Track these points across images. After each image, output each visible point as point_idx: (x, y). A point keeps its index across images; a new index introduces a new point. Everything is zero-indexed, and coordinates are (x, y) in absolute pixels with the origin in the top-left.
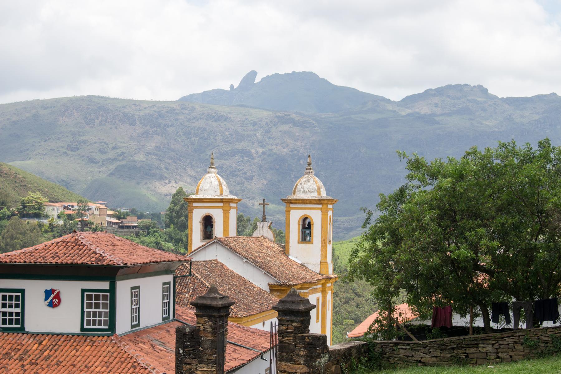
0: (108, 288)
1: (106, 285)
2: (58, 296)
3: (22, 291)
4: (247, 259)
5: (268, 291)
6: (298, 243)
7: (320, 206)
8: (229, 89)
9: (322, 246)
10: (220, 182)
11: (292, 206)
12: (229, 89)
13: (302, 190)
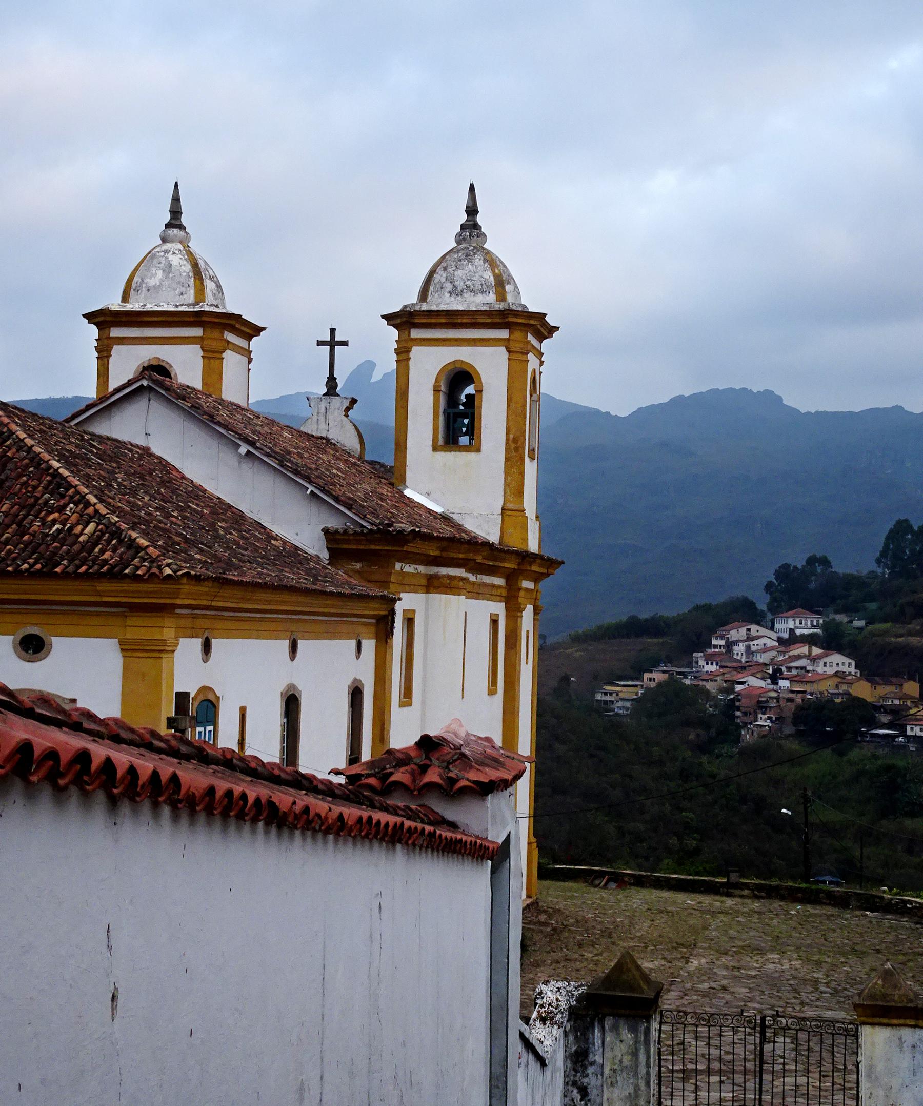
4: (252, 443)
5: (325, 555)
6: (435, 448)
7: (504, 334)
9: (507, 459)
13: (449, 287)
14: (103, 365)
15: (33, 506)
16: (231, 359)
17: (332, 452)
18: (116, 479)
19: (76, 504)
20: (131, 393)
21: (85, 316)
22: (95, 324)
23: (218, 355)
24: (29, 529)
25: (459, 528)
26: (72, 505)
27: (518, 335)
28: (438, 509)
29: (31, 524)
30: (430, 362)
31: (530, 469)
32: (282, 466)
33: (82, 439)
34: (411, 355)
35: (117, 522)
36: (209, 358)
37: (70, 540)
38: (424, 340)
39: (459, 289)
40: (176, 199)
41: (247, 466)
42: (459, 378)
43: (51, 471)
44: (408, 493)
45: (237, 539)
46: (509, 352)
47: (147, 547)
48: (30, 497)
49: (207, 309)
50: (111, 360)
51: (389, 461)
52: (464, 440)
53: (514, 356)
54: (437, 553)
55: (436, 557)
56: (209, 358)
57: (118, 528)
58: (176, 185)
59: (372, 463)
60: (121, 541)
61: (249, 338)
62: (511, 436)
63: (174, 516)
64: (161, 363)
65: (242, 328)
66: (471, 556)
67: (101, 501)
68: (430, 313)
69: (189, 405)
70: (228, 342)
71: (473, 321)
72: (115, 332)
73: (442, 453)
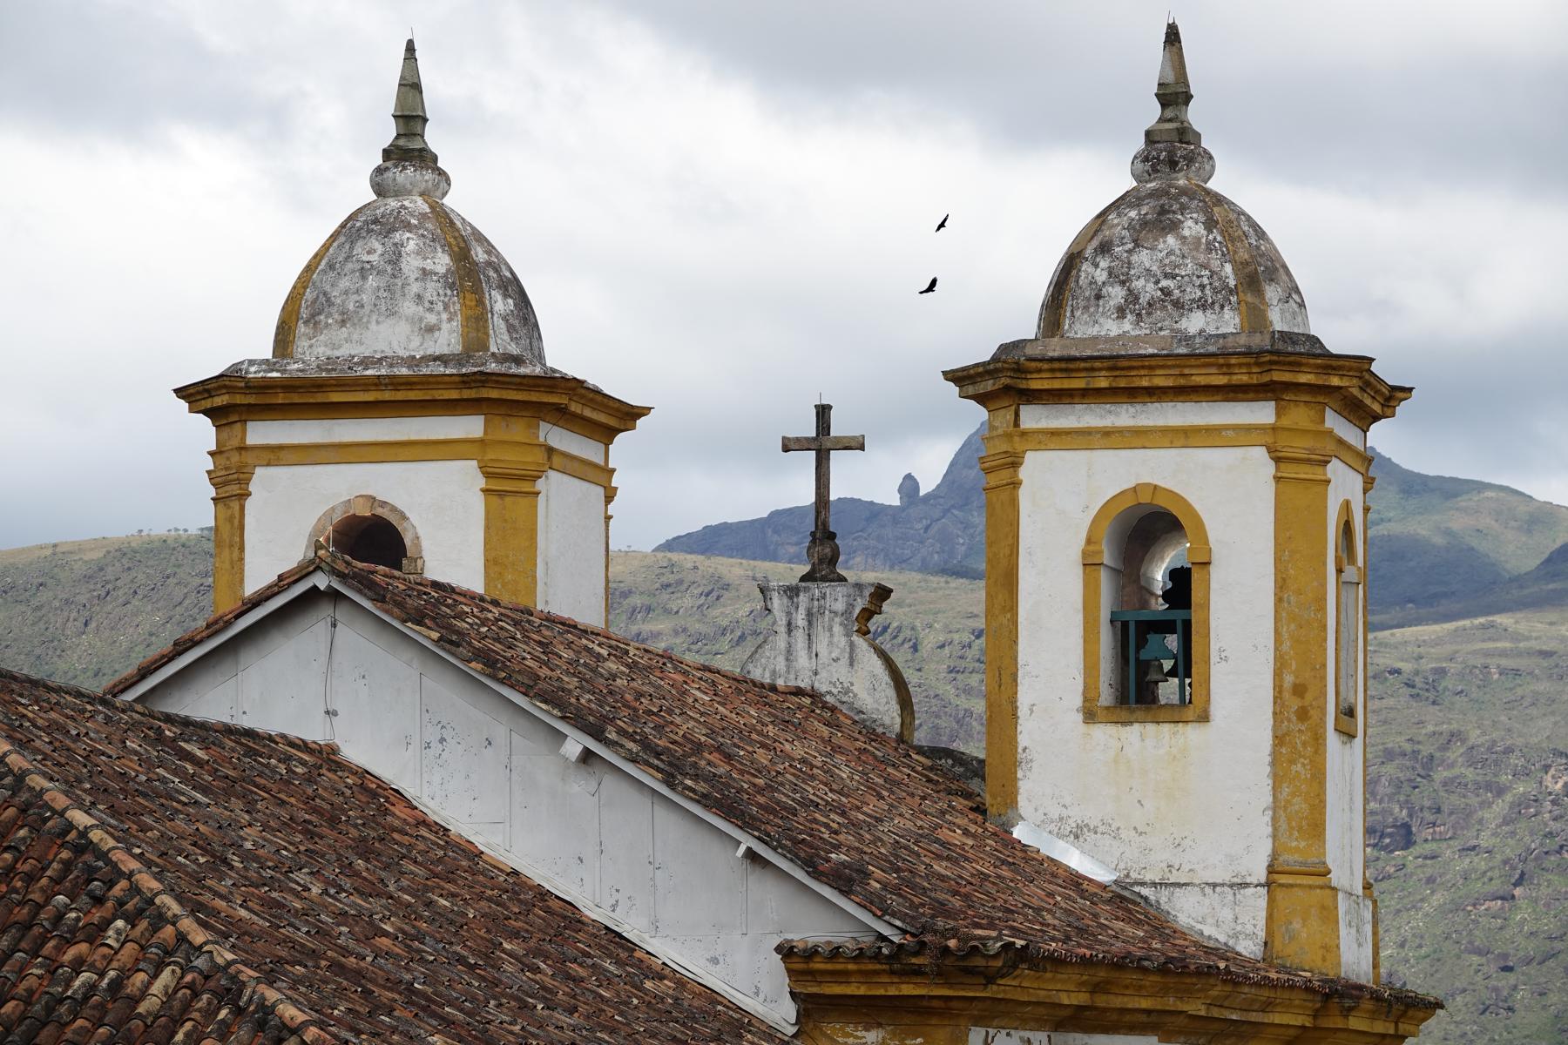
6: (1090, 714)
7: (1262, 413)
8: (894, 500)
9: (1279, 739)
11: (1034, 417)
12: (894, 500)
13: (1117, 294)
14: (230, 519)
15: (27, 926)
16: (560, 496)
17: (825, 731)
18: (237, 846)
19: (132, 921)
20: (294, 604)
21: (181, 392)
22: (206, 412)
23: (525, 487)
24: (14, 985)
25: (1160, 925)
26: (120, 923)
27: (1300, 416)
28: (1101, 874)
29: (21, 973)
30: (1066, 493)
31: (1344, 763)
32: (671, 786)
33: (160, 738)
34: (1024, 473)
35: (229, 964)
36: (501, 494)
37: (115, 1010)
38: (1055, 433)
39: (1143, 300)
40: (411, 86)
41: (580, 787)
42: (1147, 525)
43: (73, 834)
44: (1018, 833)
45: (548, 982)
46: (1278, 460)
47: (305, 1024)
48: (21, 903)
49: (493, 367)
50: (250, 504)
51: (975, 749)
52: (1168, 690)
53: (1290, 471)
54: (1080, 998)
55: (1081, 1008)
56: (501, 494)
57: (234, 978)
58: (410, 48)
59: (934, 752)
60: (239, 1011)
61: (607, 434)
62: (1289, 679)
63: (386, 934)
64: (379, 511)
65: (588, 413)
66: (1171, 1003)
67: (195, 908)
68: (1067, 364)
69: (435, 635)
70: (551, 451)
71: (1182, 382)
72: (260, 433)
73: (1112, 729)
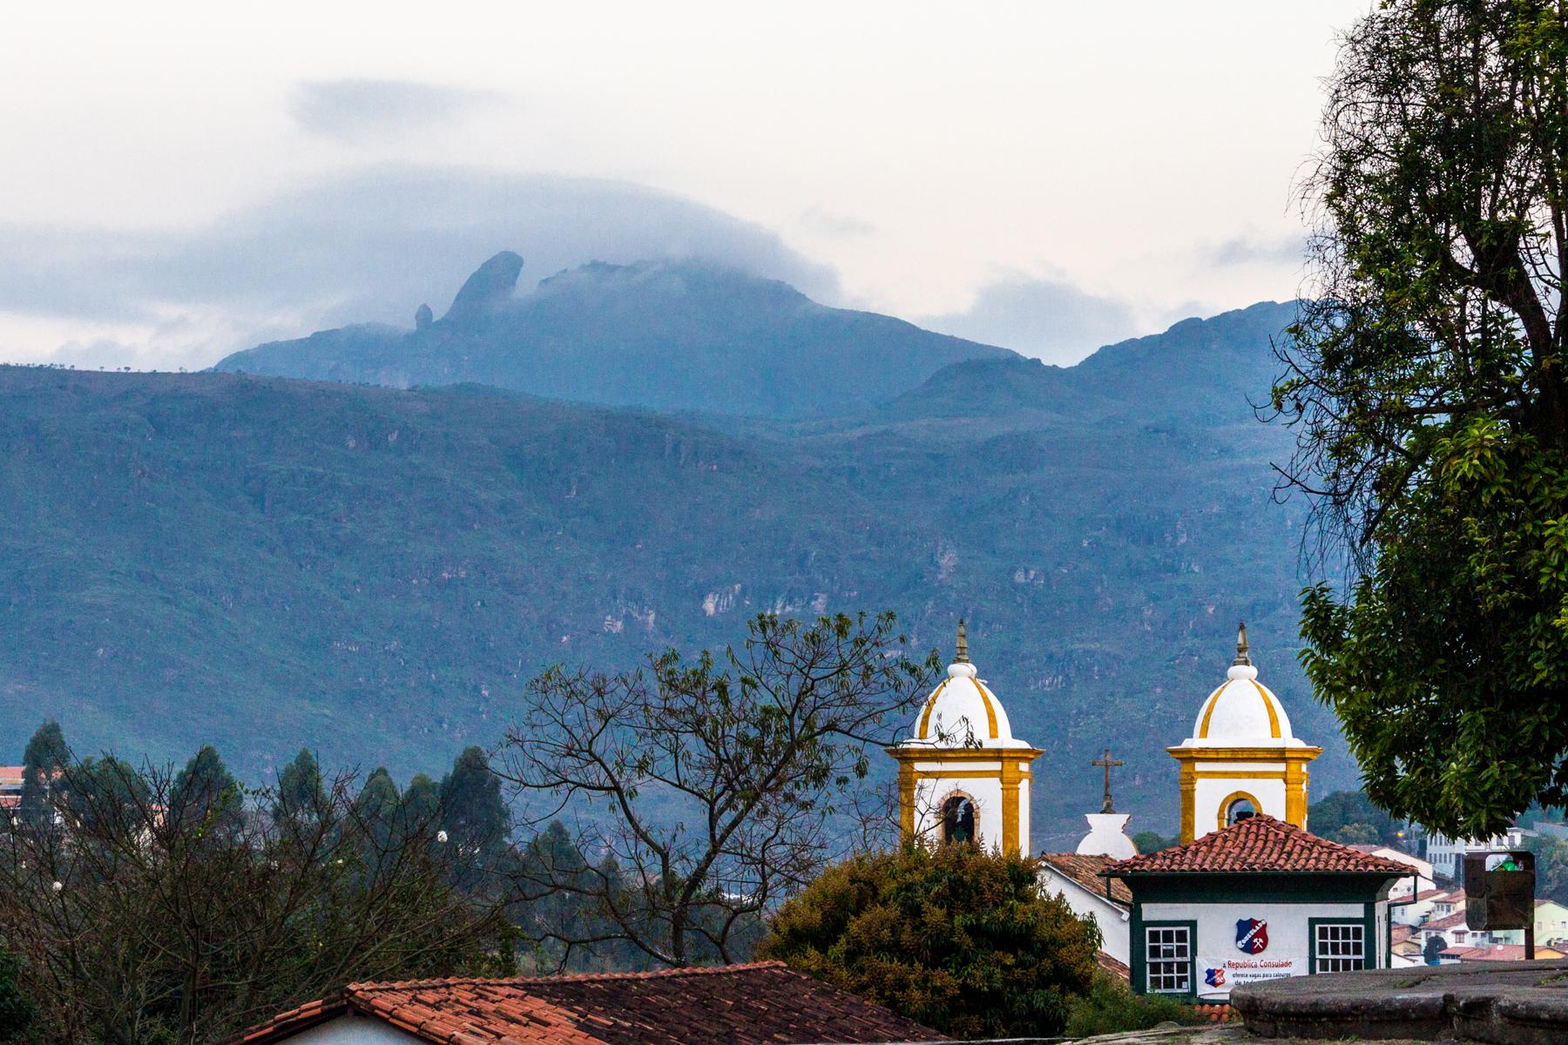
0: (1361, 915)
1: (1357, 910)
2: (1262, 934)
3: (1193, 924)
7: (1281, 767)
10: (1269, 706)
